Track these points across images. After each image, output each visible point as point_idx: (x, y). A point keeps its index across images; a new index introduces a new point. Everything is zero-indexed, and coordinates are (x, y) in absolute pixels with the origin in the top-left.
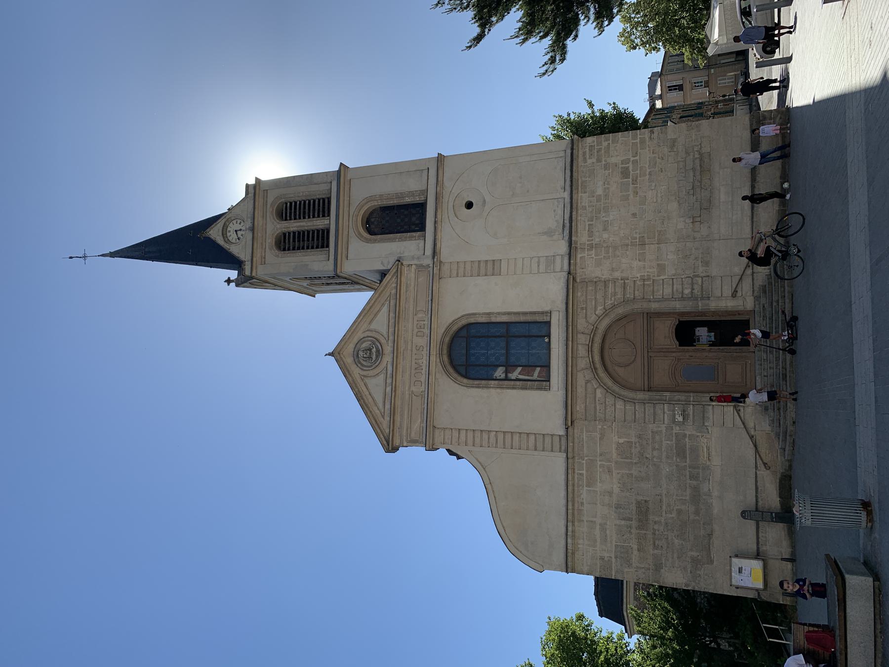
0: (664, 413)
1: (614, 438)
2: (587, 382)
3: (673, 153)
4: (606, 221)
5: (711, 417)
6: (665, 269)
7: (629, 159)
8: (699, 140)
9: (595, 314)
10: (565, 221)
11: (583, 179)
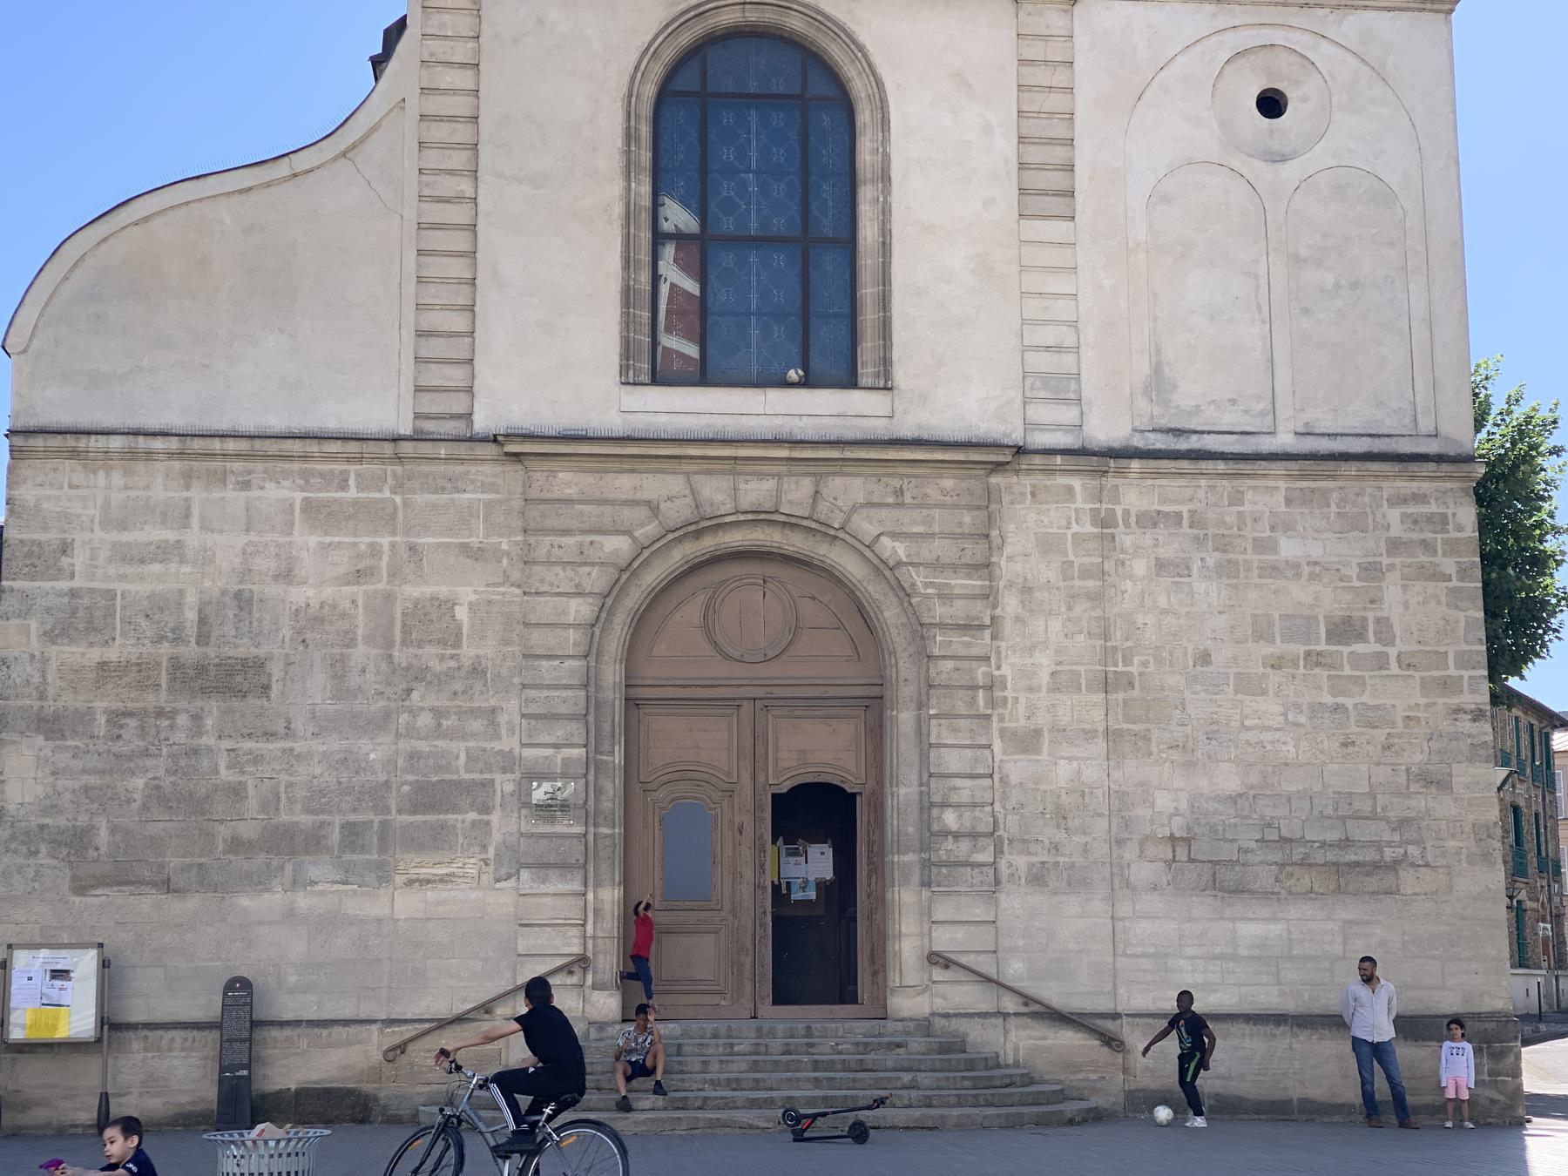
0: (556, 746)
1: (470, 589)
2: (653, 508)
3: (1402, 779)
4: (1188, 568)
5: (544, 888)
6: (1025, 751)
7: (1392, 643)
8: (1442, 862)
9: (879, 535)
10: (1194, 437)
11: (1335, 495)
